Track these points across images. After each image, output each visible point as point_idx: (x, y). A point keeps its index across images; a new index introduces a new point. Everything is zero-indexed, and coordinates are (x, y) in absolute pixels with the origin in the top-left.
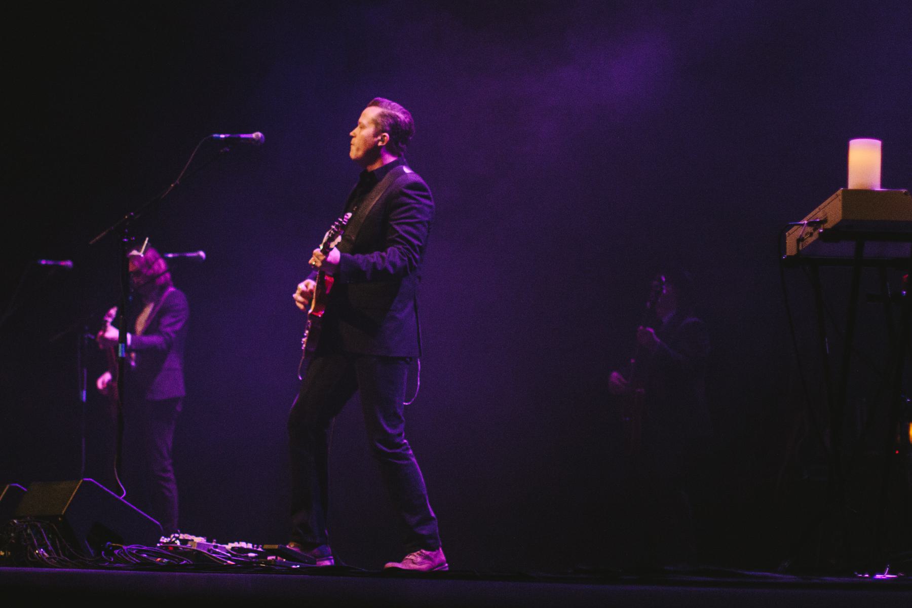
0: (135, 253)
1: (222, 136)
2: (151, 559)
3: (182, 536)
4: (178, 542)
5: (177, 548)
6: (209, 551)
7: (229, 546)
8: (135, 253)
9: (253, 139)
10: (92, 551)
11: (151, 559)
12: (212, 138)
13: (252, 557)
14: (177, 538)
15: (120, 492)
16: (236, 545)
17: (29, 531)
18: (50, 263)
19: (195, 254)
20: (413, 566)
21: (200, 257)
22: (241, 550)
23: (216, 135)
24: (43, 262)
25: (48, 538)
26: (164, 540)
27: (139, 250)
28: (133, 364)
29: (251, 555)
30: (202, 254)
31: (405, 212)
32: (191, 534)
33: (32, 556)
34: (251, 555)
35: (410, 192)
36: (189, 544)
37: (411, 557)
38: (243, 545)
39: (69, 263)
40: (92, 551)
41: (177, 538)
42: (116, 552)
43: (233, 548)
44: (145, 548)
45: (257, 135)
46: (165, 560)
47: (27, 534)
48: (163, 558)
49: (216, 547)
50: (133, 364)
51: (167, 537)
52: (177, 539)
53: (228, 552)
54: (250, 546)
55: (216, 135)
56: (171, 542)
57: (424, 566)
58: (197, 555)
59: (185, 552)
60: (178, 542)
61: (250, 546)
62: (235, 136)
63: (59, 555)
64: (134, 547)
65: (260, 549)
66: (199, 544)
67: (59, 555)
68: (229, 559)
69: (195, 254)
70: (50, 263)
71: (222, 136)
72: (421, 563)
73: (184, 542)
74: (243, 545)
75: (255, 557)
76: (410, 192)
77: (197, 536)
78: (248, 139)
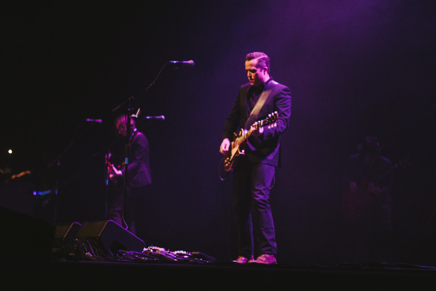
0: (133, 115)
1: (175, 62)
2: (140, 258)
3: (153, 248)
4: (152, 251)
5: (151, 253)
6: (166, 254)
7: (176, 253)
8: (133, 115)
9: (189, 64)
10: (112, 254)
11: (140, 258)
12: (182, 63)
13: (186, 258)
14: (151, 249)
15: (125, 227)
16: (178, 252)
17: (83, 244)
18: (92, 120)
19: (159, 117)
20: (261, 262)
21: (162, 118)
22: (181, 254)
23: (172, 62)
24: (88, 120)
25: (92, 247)
26: (145, 249)
27: (135, 114)
28: (241, 260)
29: (186, 257)
30: (163, 117)
31: (283, 101)
32: (158, 247)
33: (84, 255)
34: (186, 257)
35: (284, 92)
36: (157, 252)
37: (260, 258)
38: (182, 252)
39: (100, 121)
40: (112, 254)
41: (151, 249)
42: (124, 254)
43: (177, 254)
44: (137, 253)
45: (191, 62)
46: (146, 259)
47: (82, 246)
48: (145, 257)
49: (169, 253)
50: (241, 260)
51: (146, 248)
52: (151, 249)
53: (175, 255)
54: (185, 253)
55: (172, 62)
56: (148, 250)
57: (267, 263)
58: (160, 256)
59: (155, 255)
60: (152, 251)
61: (185, 253)
62: (181, 62)
63: (97, 255)
64: (132, 252)
65: (190, 254)
66: (161, 252)
67: (97, 255)
68: (175, 258)
69: (159, 117)
70: (92, 120)
71: (175, 62)
72: (265, 261)
73: (154, 250)
74: (182, 252)
75: (188, 258)
76: (284, 92)
77: (160, 247)
78: (187, 63)
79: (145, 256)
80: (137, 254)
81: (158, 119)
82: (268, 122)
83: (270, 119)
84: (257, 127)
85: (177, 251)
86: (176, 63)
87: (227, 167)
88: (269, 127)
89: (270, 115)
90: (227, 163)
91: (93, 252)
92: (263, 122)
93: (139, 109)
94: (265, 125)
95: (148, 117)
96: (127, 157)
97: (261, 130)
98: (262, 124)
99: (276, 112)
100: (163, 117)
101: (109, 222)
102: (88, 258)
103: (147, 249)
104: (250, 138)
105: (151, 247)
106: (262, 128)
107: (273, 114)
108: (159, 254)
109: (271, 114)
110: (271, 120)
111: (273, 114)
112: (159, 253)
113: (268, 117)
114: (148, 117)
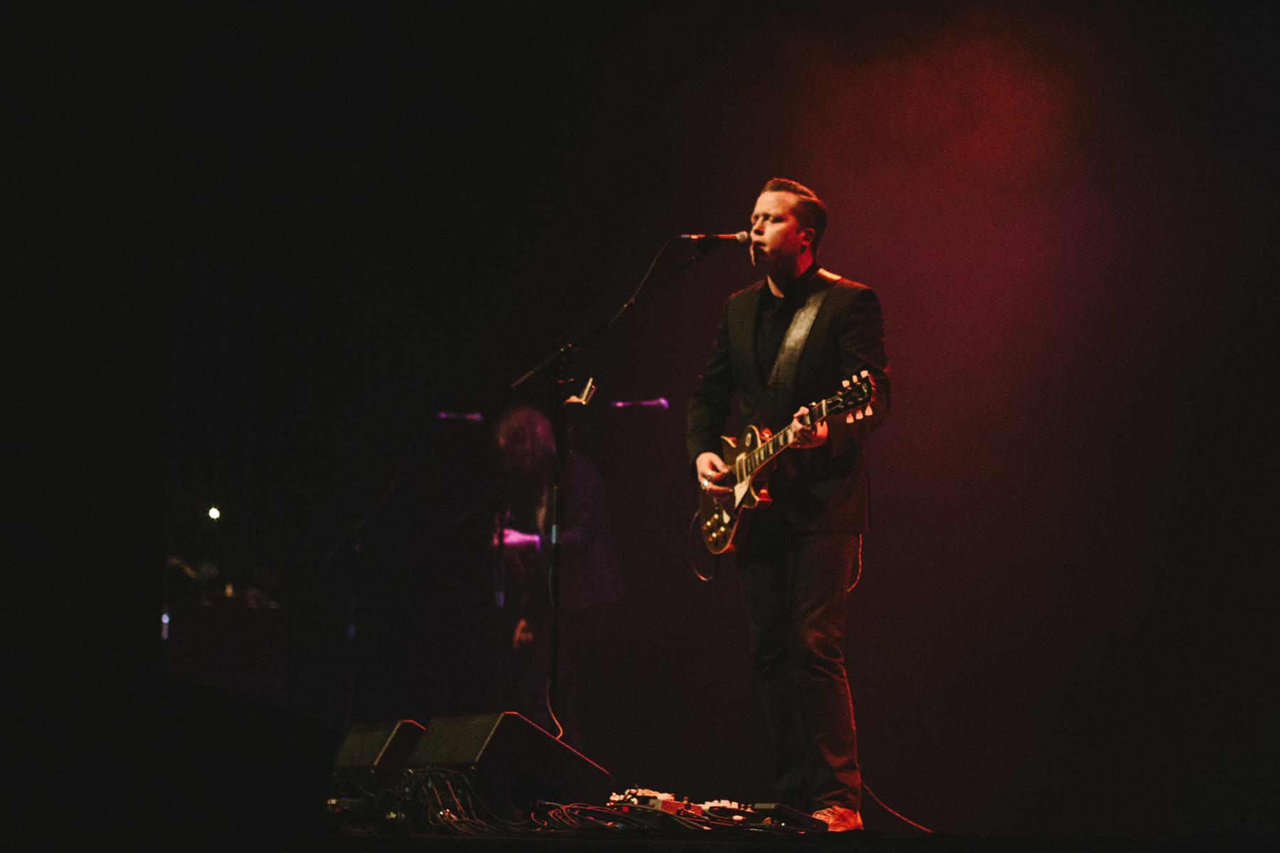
0: (574, 399)
3: (640, 792)
4: (635, 801)
5: (633, 808)
6: (678, 812)
7: (706, 806)
8: (574, 399)
13: (738, 821)
14: (634, 795)
16: (715, 804)
21: (661, 406)
25: (457, 794)
26: (615, 797)
27: (579, 396)
29: (737, 818)
33: (435, 819)
34: (737, 818)
36: (652, 802)
38: (725, 803)
41: (634, 795)
42: (551, 813)
47: (428, 790)
49: (688, 807)
51: (619, 794)
53: (704, 813)
54: (735, 805)
60: (635, 801)
61: (735, 805)
65: (749, 810)
66: (665, 803)
69: (655, 403)
73: (644, 800)
74: (725, 803)
77: (661, 792)
79: (615, 819)
83: (847, 394)
84: (808, 420)
88: (850, 420)
89: (846, 383)
90: (711, 530)
91: (460, 808)
92: (828, 406)
94: (835, 417)
95: (620, 404)
97: (822, 430)
99: (864, 374)
100: (663, 401)
101: (507, 716)
105: (633, 791)
108: (657, 812)
109: (851, 380)
110: (855, 399)
112: (659, 807)
114: (620, 404)
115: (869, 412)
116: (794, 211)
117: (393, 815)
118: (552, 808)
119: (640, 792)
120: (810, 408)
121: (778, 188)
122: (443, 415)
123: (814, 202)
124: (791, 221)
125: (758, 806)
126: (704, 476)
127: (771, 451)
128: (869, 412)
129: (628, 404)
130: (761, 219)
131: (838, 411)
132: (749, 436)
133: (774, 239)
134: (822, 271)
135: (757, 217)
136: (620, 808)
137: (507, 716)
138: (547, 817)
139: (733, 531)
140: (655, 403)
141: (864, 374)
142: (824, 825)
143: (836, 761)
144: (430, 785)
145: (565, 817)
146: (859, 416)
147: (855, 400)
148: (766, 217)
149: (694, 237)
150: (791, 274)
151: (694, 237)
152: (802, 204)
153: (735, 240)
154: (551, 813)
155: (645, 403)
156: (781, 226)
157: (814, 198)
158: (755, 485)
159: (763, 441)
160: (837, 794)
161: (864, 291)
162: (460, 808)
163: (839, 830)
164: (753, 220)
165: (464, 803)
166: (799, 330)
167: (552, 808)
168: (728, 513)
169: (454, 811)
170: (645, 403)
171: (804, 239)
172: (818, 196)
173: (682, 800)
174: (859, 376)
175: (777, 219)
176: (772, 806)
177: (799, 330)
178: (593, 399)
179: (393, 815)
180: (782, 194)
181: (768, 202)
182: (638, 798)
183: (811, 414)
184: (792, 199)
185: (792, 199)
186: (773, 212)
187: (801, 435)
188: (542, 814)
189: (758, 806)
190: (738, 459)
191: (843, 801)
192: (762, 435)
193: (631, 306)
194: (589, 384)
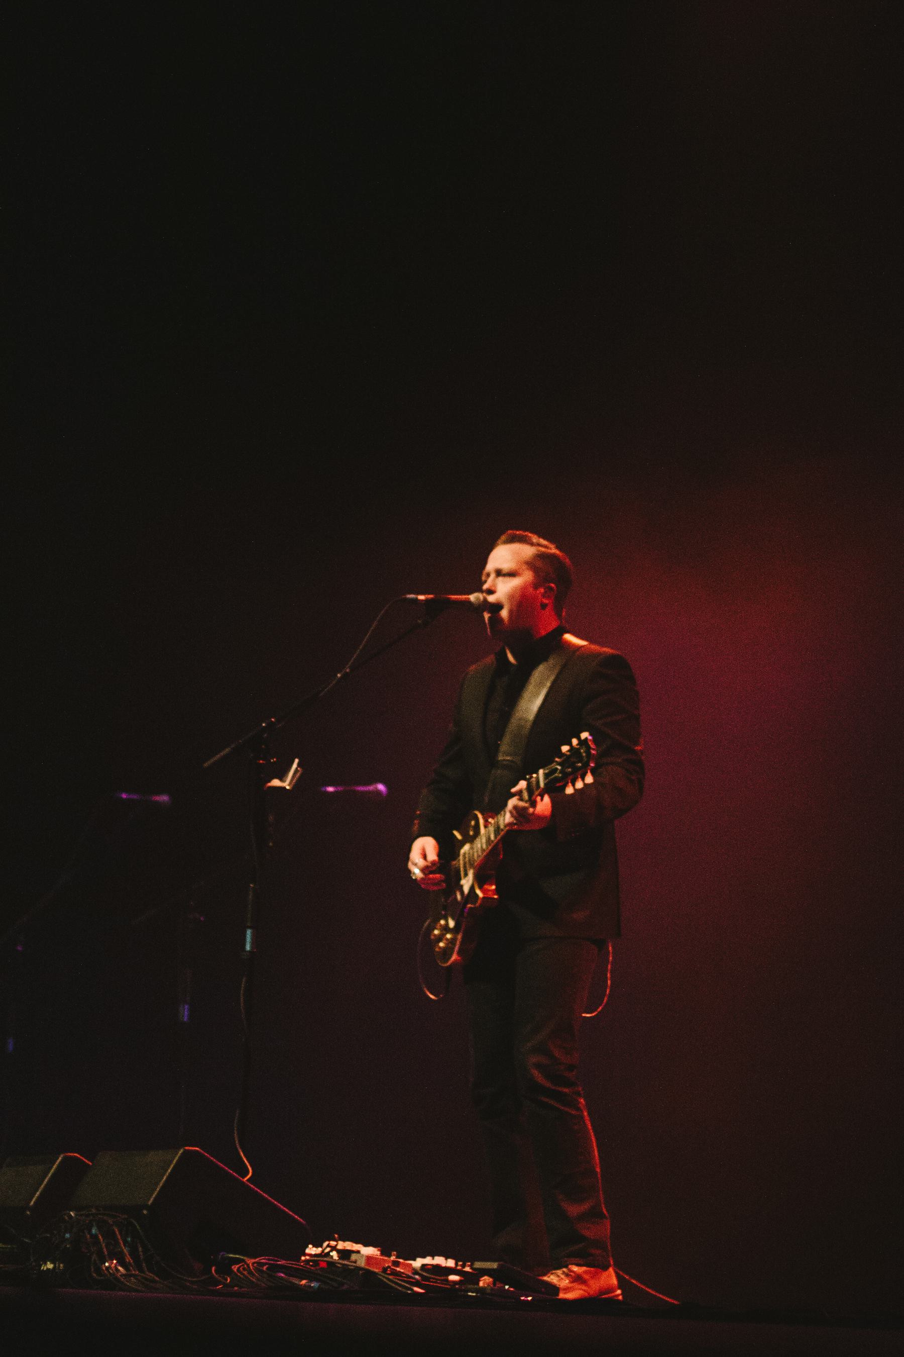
0: (276, 783)
3: (341, 1245)
4: (334, 1254)
5: (332, 1264)
6: (385, 1270)
7: (418, 1263)
8: (276, 783)
13: (455, 1282)
14: (334, 1248)
16: (428, 1260)
21: (379, 793)
22: (437, 1268)
25: (125, 1242)
26: (311, 1250)
27: (282, 779)
29: (453, 1278)
33: (98, 1270)
34: (453, 1278)
36: (354, 1257)
38: (440, 1261)
41: (334, 1248)
42: (235, 1268)
43: (423, 1266)
47: (92, 1236)
49: (396, 1264)
51: (316, 1246)
53: (415, 1272)
54: (451, 1263)
58: (366, 1280)
60: (334, 1254)
61: (451, 1263)
65: (467, 1269)
66: (369, 1258)
67: (142, 1271)
69: (371, 788)
73: (345, 1254)
74: (440, 1261)
77: (366, 1245)
79: (310, 1277)
80: (282, 1268)
81: (362, 792)
82: (561, 772)
83: (567, 761)
84: (526, 795)
85: (424, 1257)
86: (427, 600)
87: (446, 952)
88: (569, 790)
89: (565, 749)
90: (440, 938)
91: (128, 1259)
92: (546, 776)
93: (297, 761)
94: (554, 788)
95: (331, 789)
96: (250, 927)
97: (544, 805)
98: (542, 784)
99: (585, 735)
100: (381, 787)
101: (185, 1150)
102: (111, 1282)
103: (320, 1249)
104: (508, 840)
105: (333, 1243)
106: (547, 799)
107: (575, 742)
108: (360, 1269)
109: (570, 744)
110: (573, 765)
111: (575, 742)
112: (362, 1263)
113: (561, 754)
114: (331, 789)
115: (589, 779)
116: (530, 564)
117: (50, 1266)
118: (237, 1261)
119: (341, 1245)
120: (528, 780)
121: (512, 540)
122: (124, 796)
123: (553, 556)
124: (527, 576)
125: (478, 1265)
126: (416, 865)
127: (492, 837)
128: (589, 779)
129: (340, 789)
130: (493, 576)
131: (557, 780)
132: (473, 823)
133: (511, 597)
134: (568, 637)
135: (488, 575)
136: (316, 1263)
137: (185, 1150)
138: (230, 1272)
139: (459, 937)
140: (371, 788)
141: (585, 735)
142: (555, 1289)
143: (574, 1210)
144: (94, 1231)
145: (250, 1272)
146: (579, 785)
147: (574, 766)
148: (499, 573)
149: (421, 597)
150: (527, 639)
151: (421, 597)
152: (540, 556)
153: (469, 602)
154: (235, 1268)
155: (361, 788)
156: (516, 582)
157: (553, 550)
158: (480, 879)
159: (486, 827)
160: (571, 1247)
161: (613, 657)
162: (128, 1259)
163: (570, 1296)
164: (483, 578)
165: (134, 1253)
166: (532, 703)
167: (237, 1261)
168: (453, 919)
169: (122, 1262)
170: (361, 788)
171: (543, 596)
172: (557, 548)
173: (389, 1256)
174: (579, 738)
175: (512, 574)
176: (495, 1265)
177: (532, 703)
178: (298, 785)
179: (50, 1266)
180: (516, 546)
181: (503, 556)
182: (339, 1251)
183: (529, 788)
184: (527, 551)
185: (527, 551)
186: (506, 566)
187: (519, 812)
188: (225, 1268)
189: (478, 1265)
190: (462, 851)
191: (583, 1258)
192: (486, 821)
193: (345, 676)
194: (295, 766)
